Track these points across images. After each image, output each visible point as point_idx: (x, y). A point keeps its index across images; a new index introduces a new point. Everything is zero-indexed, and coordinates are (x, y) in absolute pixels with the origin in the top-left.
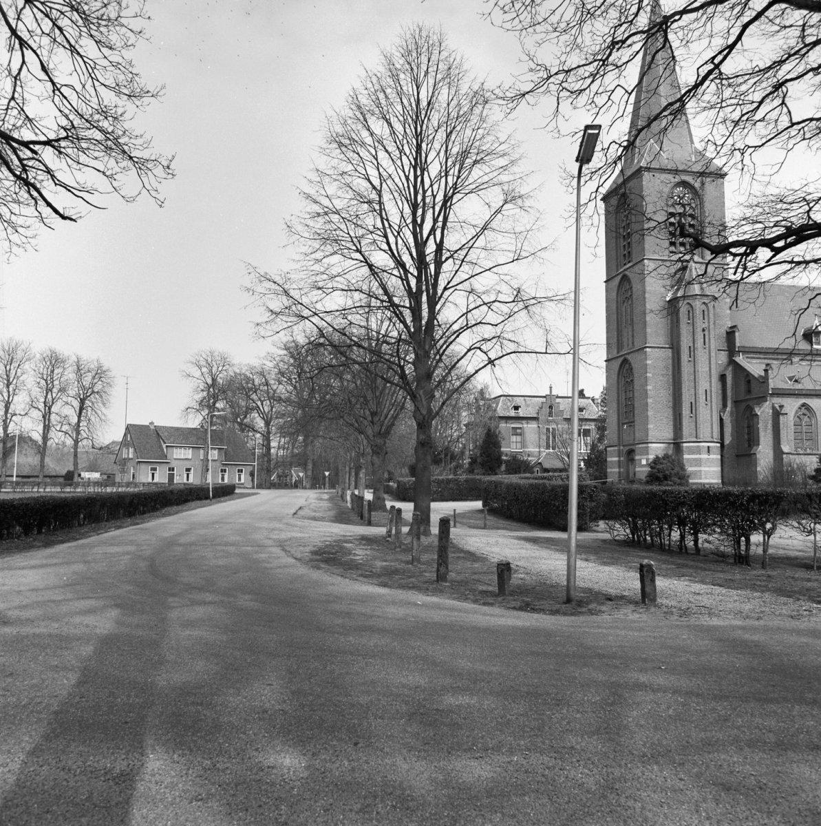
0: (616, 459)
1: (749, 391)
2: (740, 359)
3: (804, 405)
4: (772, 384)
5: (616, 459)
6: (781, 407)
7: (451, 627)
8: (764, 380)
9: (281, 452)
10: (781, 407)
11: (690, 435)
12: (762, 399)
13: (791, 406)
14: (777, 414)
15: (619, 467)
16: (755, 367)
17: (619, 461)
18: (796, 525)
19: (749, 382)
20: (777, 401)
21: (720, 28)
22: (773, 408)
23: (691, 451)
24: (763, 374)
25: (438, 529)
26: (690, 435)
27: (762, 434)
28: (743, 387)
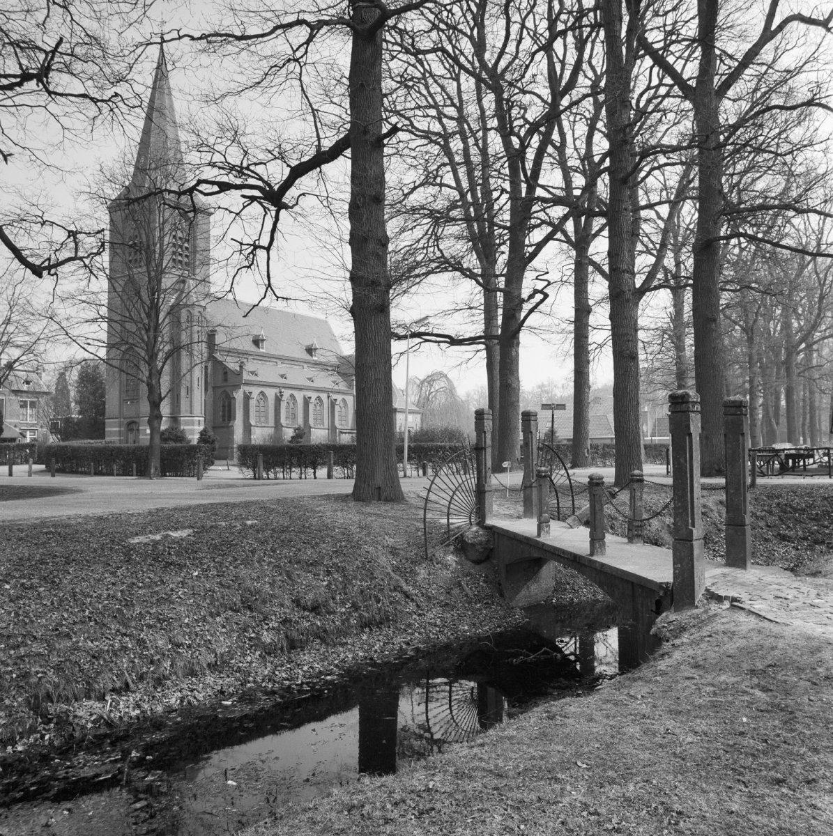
0: (117, 429)
1: (226, 380)
2: (218, 356)
3: (262, 392)
4: (246, 376)
5: (117, 429)
6: (251, 393)
7: (500, 415)
8: (239, 374)
9: (567, 639)
10: (251, 393)
11: (186, 411)
12: (237, 386)
13: (255, 391)
14: (247, 398)
15: (120, 435)
16: (232, 364)
17: (120, 431)
18: (645, 270)
19: (226, 373)
20: (247, 389)
21: (582, 133)
22: (245, 393)
23: (187, 423)
24: (238, 369)
25: (353, 343)
26: (186, 411)
27: (237, 412)
28: (220, 377)
